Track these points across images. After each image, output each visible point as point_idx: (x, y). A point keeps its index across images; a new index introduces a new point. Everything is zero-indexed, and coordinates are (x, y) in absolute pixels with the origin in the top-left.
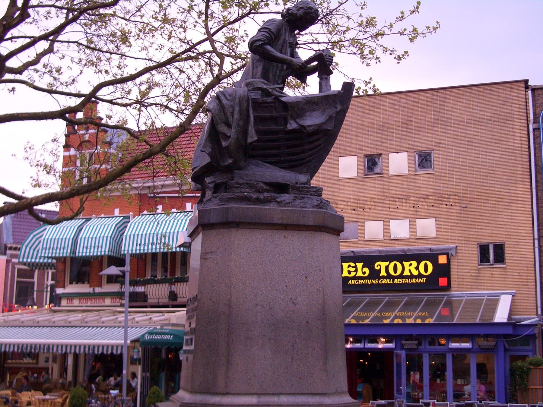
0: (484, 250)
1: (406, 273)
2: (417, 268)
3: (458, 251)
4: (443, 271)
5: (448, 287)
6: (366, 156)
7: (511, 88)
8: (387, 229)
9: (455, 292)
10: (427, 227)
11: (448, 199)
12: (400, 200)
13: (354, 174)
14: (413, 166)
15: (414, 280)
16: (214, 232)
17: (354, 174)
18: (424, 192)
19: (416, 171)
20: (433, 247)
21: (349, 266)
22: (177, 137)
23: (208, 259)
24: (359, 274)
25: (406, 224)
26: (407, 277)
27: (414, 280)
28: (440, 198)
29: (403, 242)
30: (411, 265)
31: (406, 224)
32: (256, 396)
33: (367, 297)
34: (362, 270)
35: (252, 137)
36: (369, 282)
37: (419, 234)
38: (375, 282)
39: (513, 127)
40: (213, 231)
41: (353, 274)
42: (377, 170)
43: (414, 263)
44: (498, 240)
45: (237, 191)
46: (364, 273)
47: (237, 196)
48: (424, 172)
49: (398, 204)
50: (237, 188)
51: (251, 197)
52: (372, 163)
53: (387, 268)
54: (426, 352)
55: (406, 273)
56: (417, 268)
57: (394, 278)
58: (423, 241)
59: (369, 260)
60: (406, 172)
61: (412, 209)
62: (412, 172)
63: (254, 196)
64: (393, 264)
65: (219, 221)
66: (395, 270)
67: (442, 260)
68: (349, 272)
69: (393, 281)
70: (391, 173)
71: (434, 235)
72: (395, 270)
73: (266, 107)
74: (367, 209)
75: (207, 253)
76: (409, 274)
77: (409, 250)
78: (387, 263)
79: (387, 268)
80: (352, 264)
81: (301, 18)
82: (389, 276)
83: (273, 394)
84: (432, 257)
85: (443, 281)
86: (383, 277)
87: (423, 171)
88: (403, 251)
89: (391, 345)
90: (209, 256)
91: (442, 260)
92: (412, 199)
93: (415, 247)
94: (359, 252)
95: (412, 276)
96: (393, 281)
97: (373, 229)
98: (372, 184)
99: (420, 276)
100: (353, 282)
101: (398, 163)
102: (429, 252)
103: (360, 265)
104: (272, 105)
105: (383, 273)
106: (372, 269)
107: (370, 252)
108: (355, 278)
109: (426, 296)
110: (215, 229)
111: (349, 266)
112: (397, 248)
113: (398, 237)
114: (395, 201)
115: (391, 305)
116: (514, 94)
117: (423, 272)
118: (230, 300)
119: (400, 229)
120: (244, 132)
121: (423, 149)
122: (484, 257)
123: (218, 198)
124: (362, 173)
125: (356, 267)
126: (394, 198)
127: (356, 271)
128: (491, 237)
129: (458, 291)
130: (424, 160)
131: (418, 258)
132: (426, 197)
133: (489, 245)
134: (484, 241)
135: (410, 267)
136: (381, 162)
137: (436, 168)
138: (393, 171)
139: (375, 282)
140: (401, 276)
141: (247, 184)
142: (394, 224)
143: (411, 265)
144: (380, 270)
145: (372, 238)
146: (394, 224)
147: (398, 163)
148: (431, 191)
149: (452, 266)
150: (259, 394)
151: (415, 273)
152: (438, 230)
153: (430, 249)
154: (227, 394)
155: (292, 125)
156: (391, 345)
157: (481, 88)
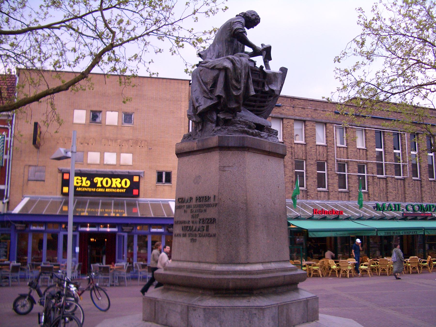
0: (160, 175)
1: (114, 185)
2: (120, 183)
3: (145, 174)
4: (135, 185)
5: (138, 196)
6: (92, 111)
7: (182, 83)
8: (102, 158)
9: (141, 199)
10: (127, 158)
11: (141, 143)
12: (112, 140)
13: (83, 122)
14: (121, 120)
15: (118, 190)
16: (230, 153)
17: (83, 122)
18: (127, 137)
19: (122, 124)
20: (130, 171)
21: (78, 179)
22: (78, 81)
23: (225, 171)
24: (84, 184)
25: (114, 155)
26: (114, 188)
27: (118, 190)
28: (136, 142)
29: (112, 167)
30: (116, 181)
31: (114, 155)
32: (261, 264)
33: (89, 199)
34: (86, 182)
35: (253, 93)
36: (90, 190)
37: (122, 162)
38: (94, 190)
39: (181, 106)
40: (229, 151)
41: (79, 184)
42: (98, 120)
43: (119, 180)
44: (168, 170)
45: (239, 126)
46: (87, 184)
47: (240, 130)
48: (127, 125)
49: (110, 143)
50: (238, 124)
51: (249, 131)
52: (95, 116)
53: (102, 182)
54: (136, 234)
55: (114, 185)
56: (120, 183)
57: (105, 188)
58: (124, 167)
59: (90, 176)
60: (116, 124)
61: (118, 147)
62: (120, 124)
63: (251, 131)
64: (105, 179)
65: (236, 145)
66: (107, 183)
67: (136, 179)
68: (77, 183)
69: (105, 190)
70: (107, 123)
71: (131, 163)
72: (107, 183)
73: (255, 73)
74: (90, 144)
75: (224, 167)
76: (115, 186)
77: (116, 172)
78: (102, 179)
79: (102, 182)
80: (80, 178)
81: (251, 20)
82: (103, 187)
83: (268, 262)
84: (130, 177)
85: (135, 192)
86: (99, 187)
87: (126, 125)
88: (112, 172)
89: (115, 230)
90: (227, 169)
91: (136, 179)
92: (119, 141)
93: (119, 170)
94: (84, 171)
95: (117, 188)
96: (105, 190)
97: (93, 157)
98: (94, 129)
99: (122, 188)
100: (79, 189)
101: (112, 118)
102: (127, 174)
103: (84, 179)
104: (258, 73)
105: (99, 185)
106: (92, 182)
107: (90, 171)
108: (81, 187)
109: (125, 200)
110: (231, 150)
111: (78, 179)
112: (108, 170)
113: (109, 163)
114: (108, 140)
115: (106, 205)
116: (183, 87)
117: (124, 185)
118: (246, 200)
119: (110, 158)
120: (247, 88)
121: (128, 111)
122: (159, 179)
123: (227, 129)
124: (88, 121)
125: (82, 180)
126: (108, 139)
127: (82, 182)
128: (164, 168)
129: (143, 198)
130: (128, 118)
131: (121, 177)
132: (128, 141)
133: (162, 172)
134: (161, 170)
135: (116, 182)
136: (100, 116)
137: (135, 124)
138: (76, 121)
139: (94, 190)
140: (110, 187)
141: (244, 122)
142: (107, 155)
143: (116, 181)
144: (97, 183)
145: (92, 162)
146: (107, 155)
147: (112, 118)
148: (131, 137)
149: (141, 183)
150: (262, 263)
151: (119, 186)
152: (133, 161)
153: (129, 172)
154: (248, 263)
155: (267, 89)
156: (115, 230)
157: (165, 81)
